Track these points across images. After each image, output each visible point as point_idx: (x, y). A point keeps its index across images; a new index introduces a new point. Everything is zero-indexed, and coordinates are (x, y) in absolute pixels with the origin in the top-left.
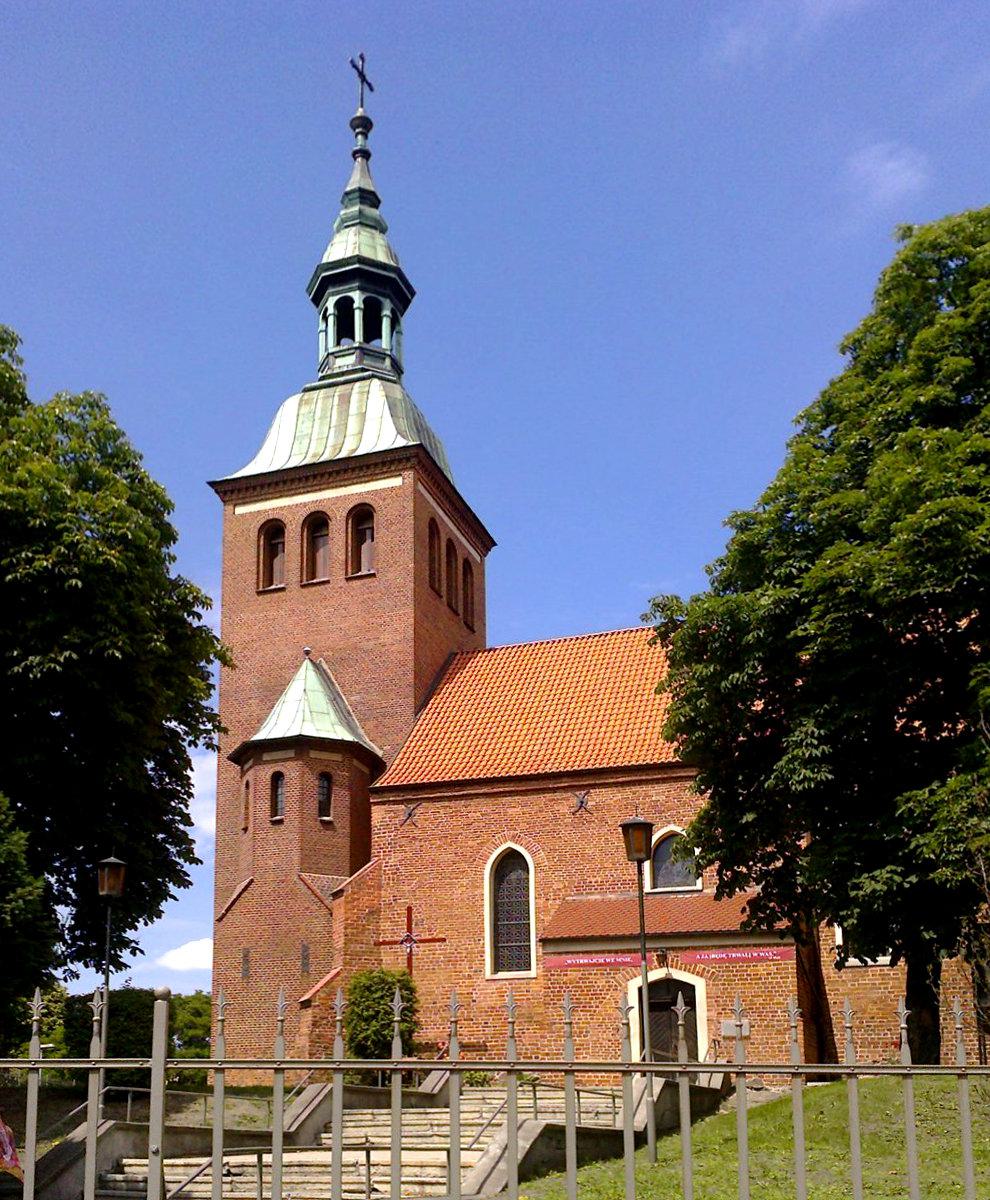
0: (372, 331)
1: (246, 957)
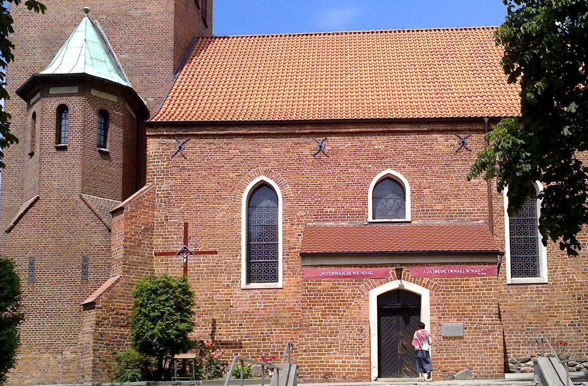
1: (31, 264)
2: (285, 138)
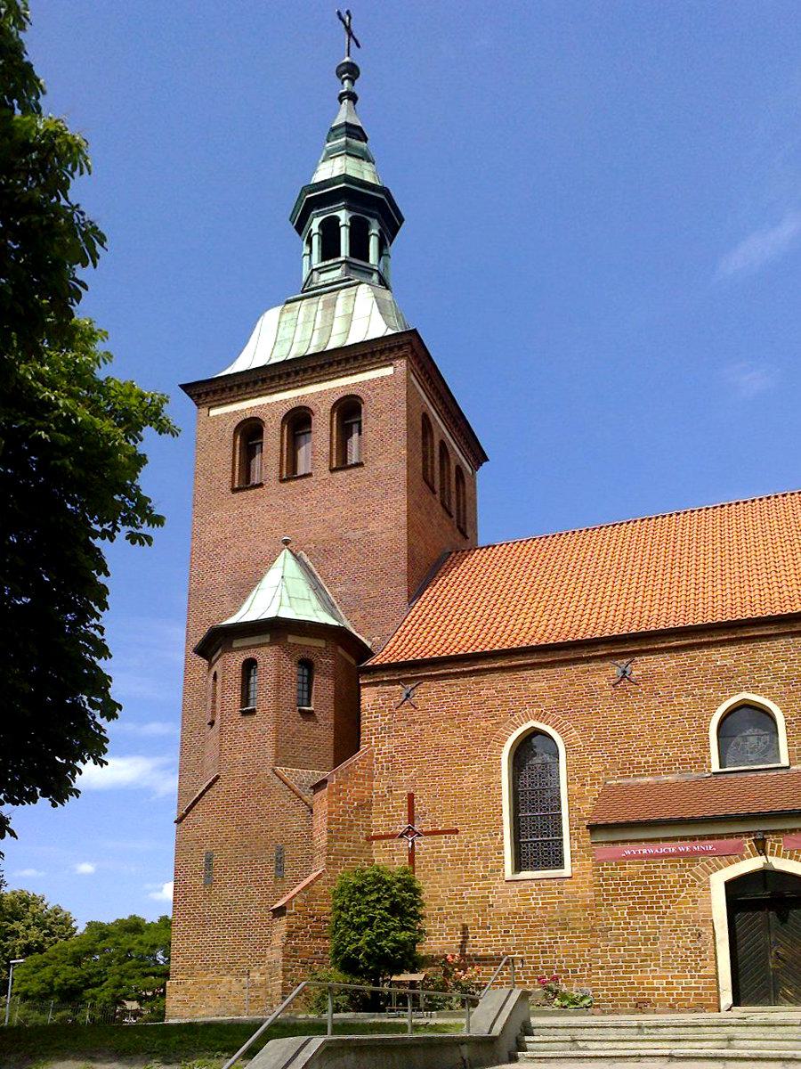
0: (359, 249)
1: (209, 860)
2: (566, 666)
